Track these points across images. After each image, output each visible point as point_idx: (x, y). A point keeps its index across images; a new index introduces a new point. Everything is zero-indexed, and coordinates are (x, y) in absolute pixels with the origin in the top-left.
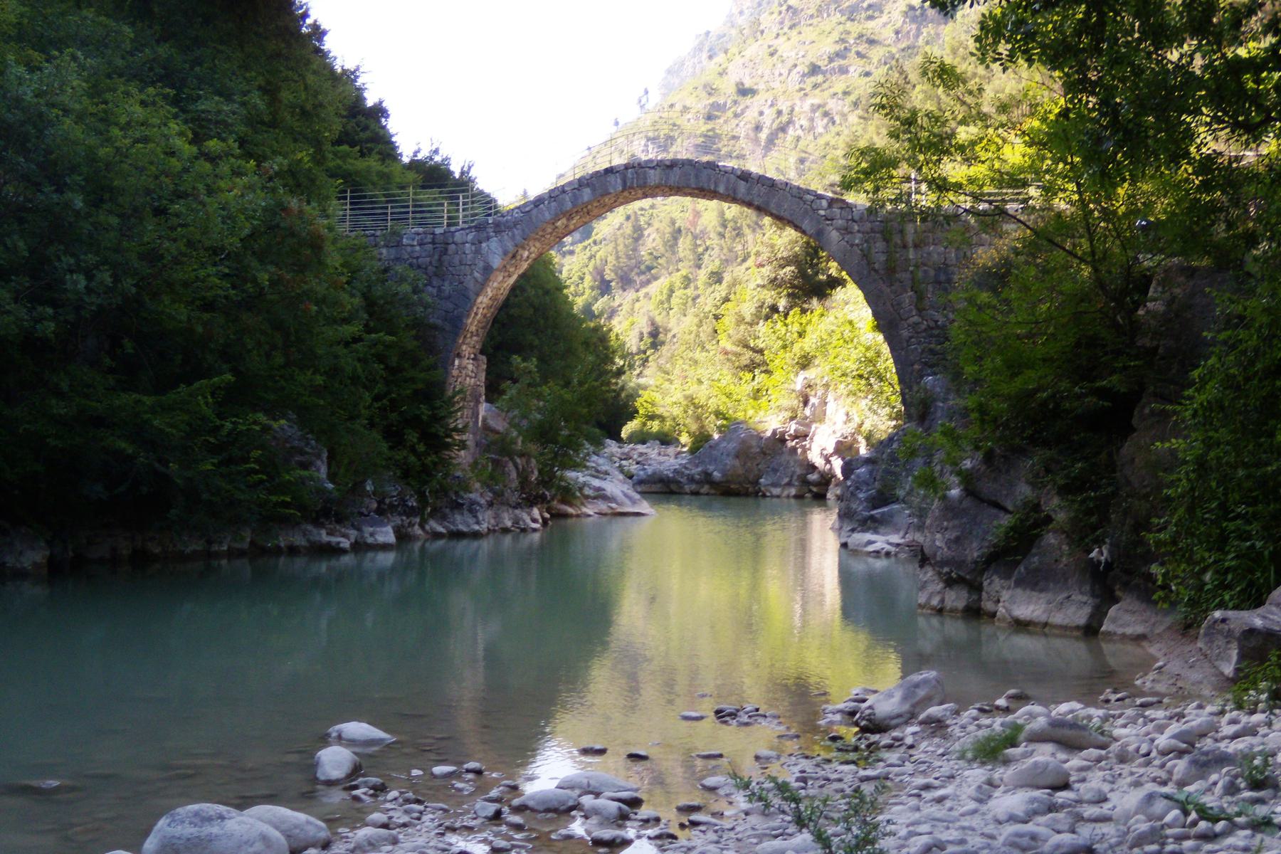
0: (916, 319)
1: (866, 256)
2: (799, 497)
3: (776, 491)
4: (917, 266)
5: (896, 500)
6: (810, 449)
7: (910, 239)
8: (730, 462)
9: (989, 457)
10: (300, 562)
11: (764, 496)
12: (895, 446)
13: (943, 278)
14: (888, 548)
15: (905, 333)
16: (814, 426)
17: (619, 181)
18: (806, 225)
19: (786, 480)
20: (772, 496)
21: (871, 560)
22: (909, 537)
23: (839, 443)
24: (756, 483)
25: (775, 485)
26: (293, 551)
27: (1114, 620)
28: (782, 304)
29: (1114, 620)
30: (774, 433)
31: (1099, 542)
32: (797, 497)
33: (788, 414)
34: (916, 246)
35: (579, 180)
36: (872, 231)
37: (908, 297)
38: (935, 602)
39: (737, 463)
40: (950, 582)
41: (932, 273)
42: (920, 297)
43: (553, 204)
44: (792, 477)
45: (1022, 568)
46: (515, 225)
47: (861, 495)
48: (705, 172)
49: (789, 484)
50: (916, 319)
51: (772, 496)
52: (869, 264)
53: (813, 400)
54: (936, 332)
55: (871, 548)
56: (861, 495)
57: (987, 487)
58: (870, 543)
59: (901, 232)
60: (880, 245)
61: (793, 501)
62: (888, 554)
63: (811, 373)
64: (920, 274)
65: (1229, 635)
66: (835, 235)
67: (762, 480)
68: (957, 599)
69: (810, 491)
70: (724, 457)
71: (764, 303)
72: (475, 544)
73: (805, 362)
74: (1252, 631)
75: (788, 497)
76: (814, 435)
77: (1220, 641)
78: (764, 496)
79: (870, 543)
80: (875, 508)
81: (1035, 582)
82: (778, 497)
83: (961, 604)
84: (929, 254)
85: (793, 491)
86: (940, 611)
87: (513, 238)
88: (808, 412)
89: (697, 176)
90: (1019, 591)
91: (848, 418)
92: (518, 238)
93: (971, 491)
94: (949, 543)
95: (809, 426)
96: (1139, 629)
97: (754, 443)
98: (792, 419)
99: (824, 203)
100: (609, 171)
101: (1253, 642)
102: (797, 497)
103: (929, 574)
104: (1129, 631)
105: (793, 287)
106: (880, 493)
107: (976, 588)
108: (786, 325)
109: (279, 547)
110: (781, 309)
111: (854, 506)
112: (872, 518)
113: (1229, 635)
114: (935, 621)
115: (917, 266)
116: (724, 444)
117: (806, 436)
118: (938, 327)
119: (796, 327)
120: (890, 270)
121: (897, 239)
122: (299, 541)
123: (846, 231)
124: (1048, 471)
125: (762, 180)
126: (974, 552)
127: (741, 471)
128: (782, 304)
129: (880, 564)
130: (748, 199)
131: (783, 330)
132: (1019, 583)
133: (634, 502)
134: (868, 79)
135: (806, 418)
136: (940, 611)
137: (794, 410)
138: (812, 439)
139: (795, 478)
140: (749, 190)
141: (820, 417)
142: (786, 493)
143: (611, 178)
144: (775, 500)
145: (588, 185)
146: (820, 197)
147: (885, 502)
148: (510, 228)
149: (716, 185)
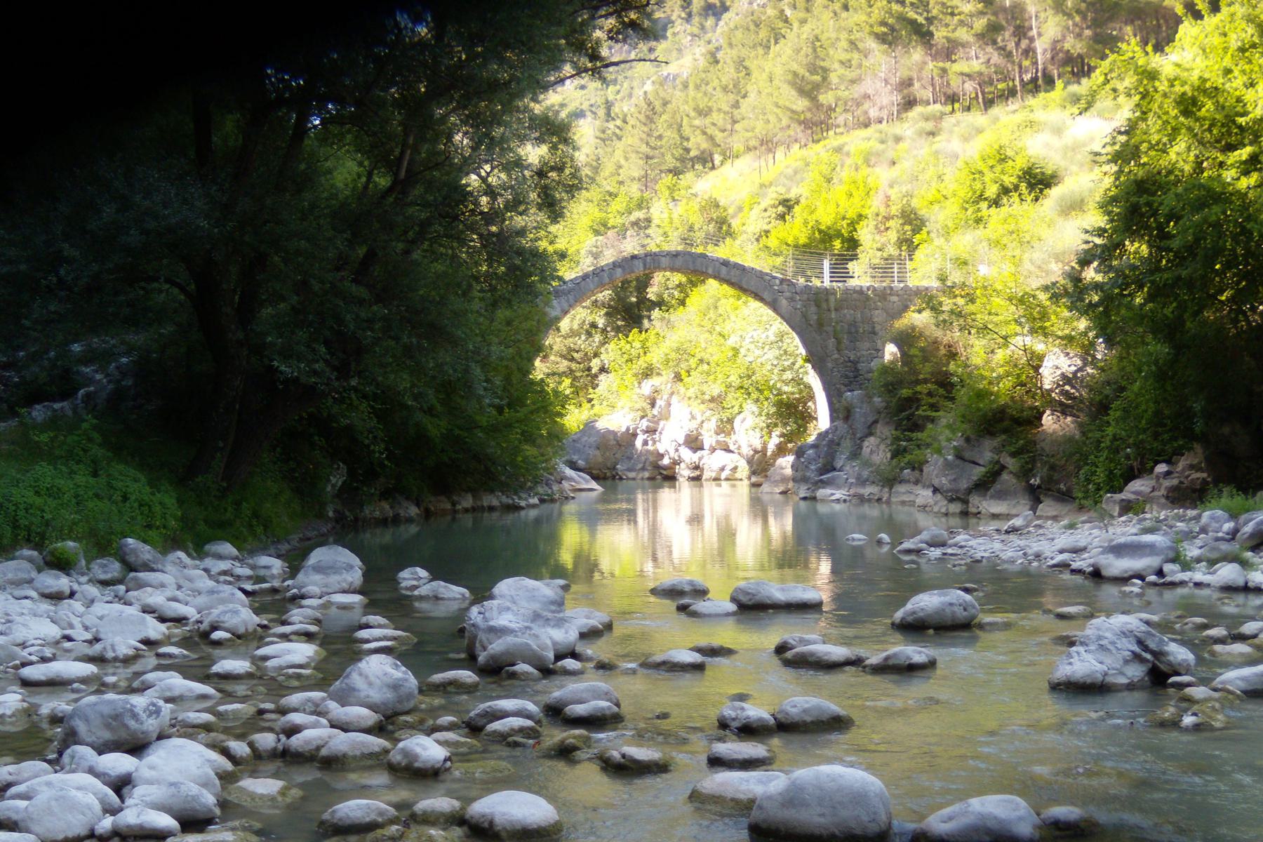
0: (836, 356)
1: (804, 316)
2: (651, 479)
3: (632, 475)
4: (837, 323)
5: (834, 469)
6: (660, 441)
7: (832, 305)
8: (593, 453)
9: (968, 440)
10: (495, 515)
11: (621, 479)
12: (830, 436)
13: (853, 330)
14: (844, 497)
15: (830, 365)
16: (662, 423)
17: (641, 265)
18: (766, 295)
19: (640, 466)
20: (628, 479)
21: (833, 504)
22: (852, 491)
23: (688, 436)
24: (614, 468)
25: (630, 470)
26: (491, 509)
27: (1041, 510)
28: (601, 322)
29: (1041, 510)
30: (628, 429)
31: (1034, 476)
32: (650, 479)
33: (641, 413)
34: (836, 310)
35: (614, 263)
36: (808, 300)
37: (831, 342)
38: (943, 510)
39: (597, 452)
40: (951, 500)
41: (846, 326)
42: (839, 342)
43: (596, 279)
44: (645, 463)
45: (992, 490)
46: (569, 292)
47: (813, 467)
48: (700, 260)
49: (643, 469)
50: (836, 356)
51: (628, 479)
52: (806, 320)
53: (659, 403)
54: (849, 364)
55: (833, 498)
56: (813, 467)
57: (967, 455)
58: (833, 494)
59: (827, 300)
60: (813, 309)
61: (647, 482)
62: (845, 501)
63: (655, 381)
64: (838, 328)
65: (1115, 502)
66: (784, 302)
67: (618, 466)
68: (956, 508)
69: (661, 474)
70: (587, 448)
71: (584, 321)
72: (552, 505)
73: (648, 373)
74: (1123, 500)
75: (642, 479)
76: (662, 429)
77: (1111, 504)
78: (621, 479)
79: (833, 494)
80: (821, 475)
81: (1001, 496)
82: (634, 479)
83: (958, 510)
84: (845, 315)
85: (647, 474)
86: (946, 514)
87: (568, 301)
88: (655, 411)
89: (694, 262)
90: (992, 501)
91: (693, 417)
92: (572, 301)
93: (959, 457)
94: (950, 481)
95: (657, 423)
96: (1054, 513)
97: (612, 437)
98: (642, 417)
99: (777, 282)
100: (634, 257)
101: (1124, 504)
102: (650, 479)
103: (939, 496)
104: (1049, 514)
105: (610, 307)
106: (824, 465)
107: (966, 502)
108: (628, 342)
109: (483, 506)
110: (600, 326)
111: (808, 474)
112: (821, 481)
113: (1115, 502)
114: (944, 520)
115: (837, 323)
116: (586, 438)
117: (656, 431)
118: (850, 361)
119: (637, 344)
120: (820, 324)
121: (824, 306)
122: (495, 503)
123: (791, 299)
124: (1004, 446)
125: (736, 266)
126: (964, 484)
127: (600, 460)
128: (601, 322)
129: (837, 507)
130: (727, 278)
131: (628, 346)
132: (992, 497)
133: (587, 481)
134: (584, 92)
135: (654, 416)
136: (946, 514)
137: (643, 410)
138: (661, 433)
139: (647, 464)
140: (728, 273)
141: (665, 415)
142: (640, 475)
143: (636, 262)
144: (631, 482)
145: (620, 266)
146: (775, 278)
147: (828, 471)
148: (566, 295)
149: (707, 268)
